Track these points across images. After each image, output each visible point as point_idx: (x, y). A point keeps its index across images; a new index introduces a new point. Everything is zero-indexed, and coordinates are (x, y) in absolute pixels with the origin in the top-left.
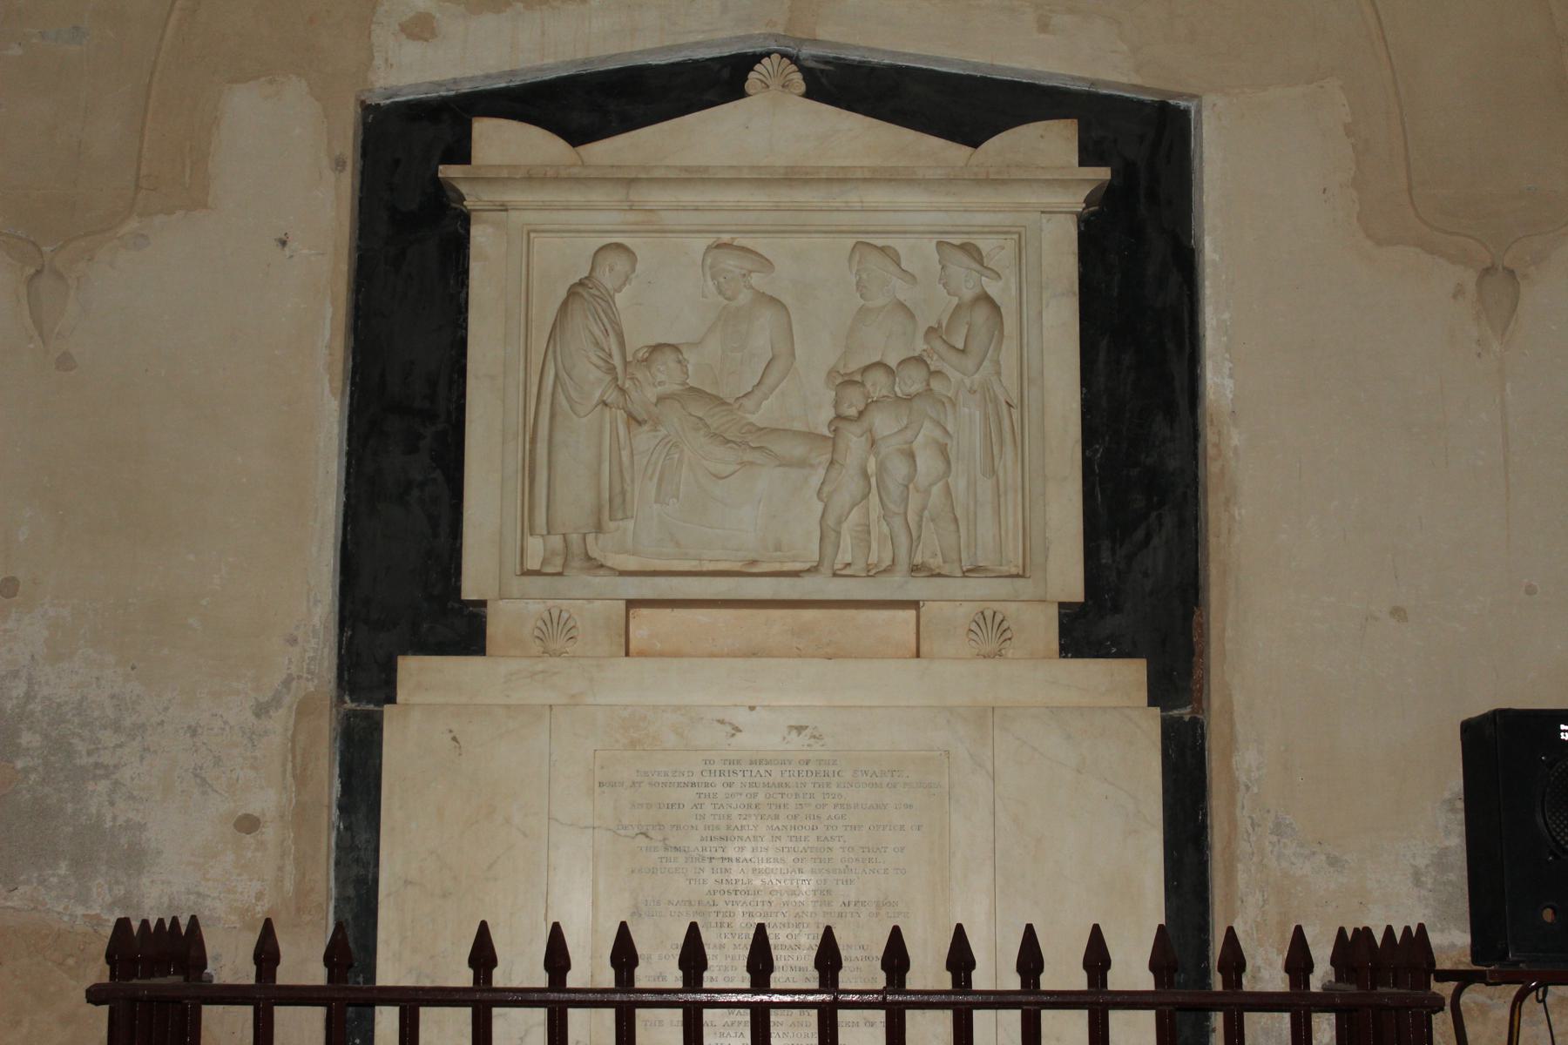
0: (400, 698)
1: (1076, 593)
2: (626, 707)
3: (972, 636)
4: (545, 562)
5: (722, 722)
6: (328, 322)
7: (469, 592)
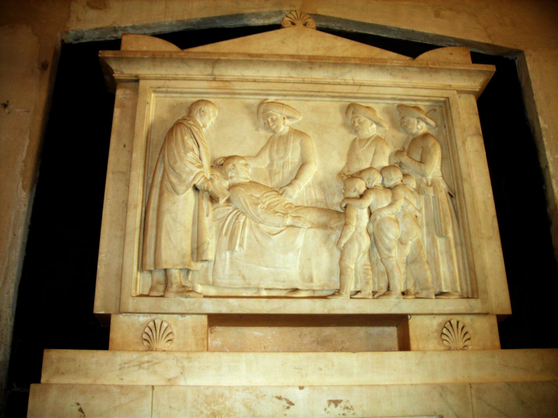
0: (43, 380)
1: (506, 308)
2: (208, 387)
3: (444, 337)
4: (152, 289)
5: (280, 398)
6: (26, 149)
7: (99, 308)
